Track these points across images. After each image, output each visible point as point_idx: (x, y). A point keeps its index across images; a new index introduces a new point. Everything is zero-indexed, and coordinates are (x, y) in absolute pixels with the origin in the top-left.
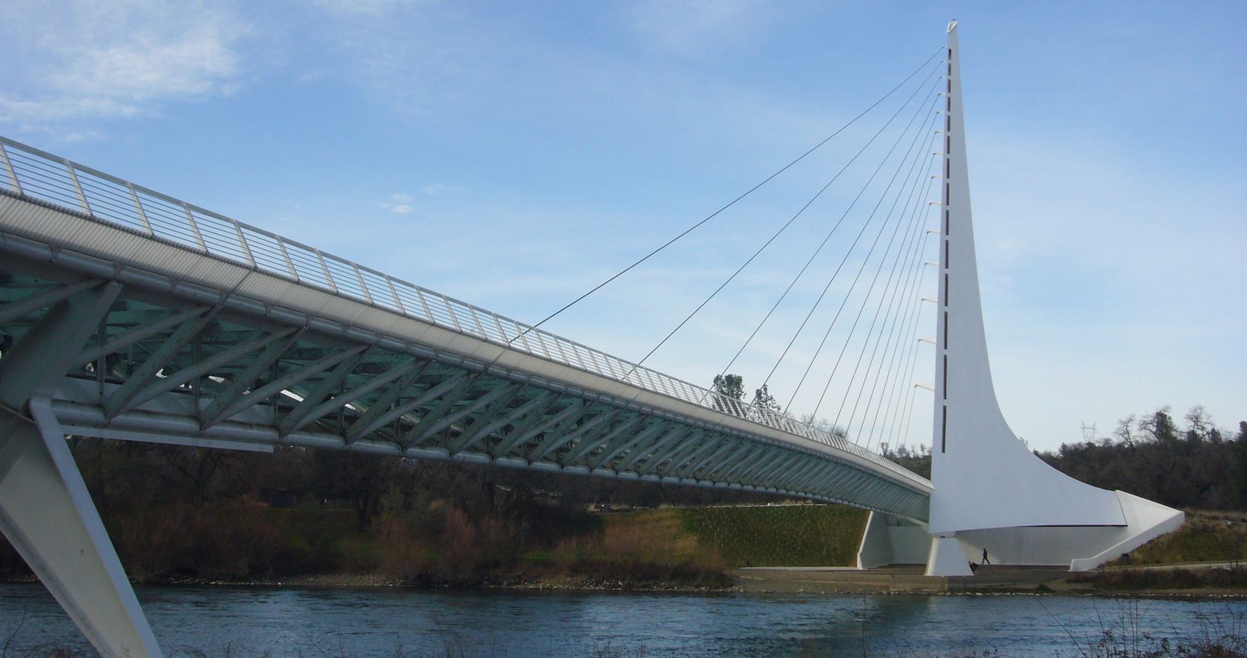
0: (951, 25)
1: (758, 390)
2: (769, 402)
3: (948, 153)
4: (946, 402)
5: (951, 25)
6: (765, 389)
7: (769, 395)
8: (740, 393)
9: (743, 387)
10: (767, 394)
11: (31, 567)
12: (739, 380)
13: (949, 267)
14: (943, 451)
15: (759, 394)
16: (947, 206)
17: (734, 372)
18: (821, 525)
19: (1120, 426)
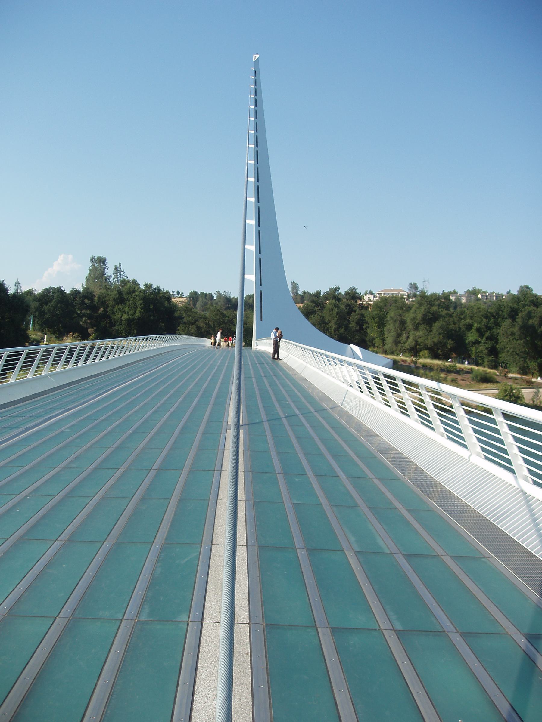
0: (255, 57)
1: (116, 266)
2: (122, 273)
3: (258, 202)
4: (261, 288)
5: (255, 57)
6: (120, 266)
7: (122, 269)
8: (105, 267)
9: (107, 263)
10: (121, 269)
11: (339, 537)
12: (105, 260)
13: (258, 146)
14: (261, 320)
15: (116, 268)
16: (257, 121)
17: (103, 255)
18: (135, 313)
19: (505, 293)
